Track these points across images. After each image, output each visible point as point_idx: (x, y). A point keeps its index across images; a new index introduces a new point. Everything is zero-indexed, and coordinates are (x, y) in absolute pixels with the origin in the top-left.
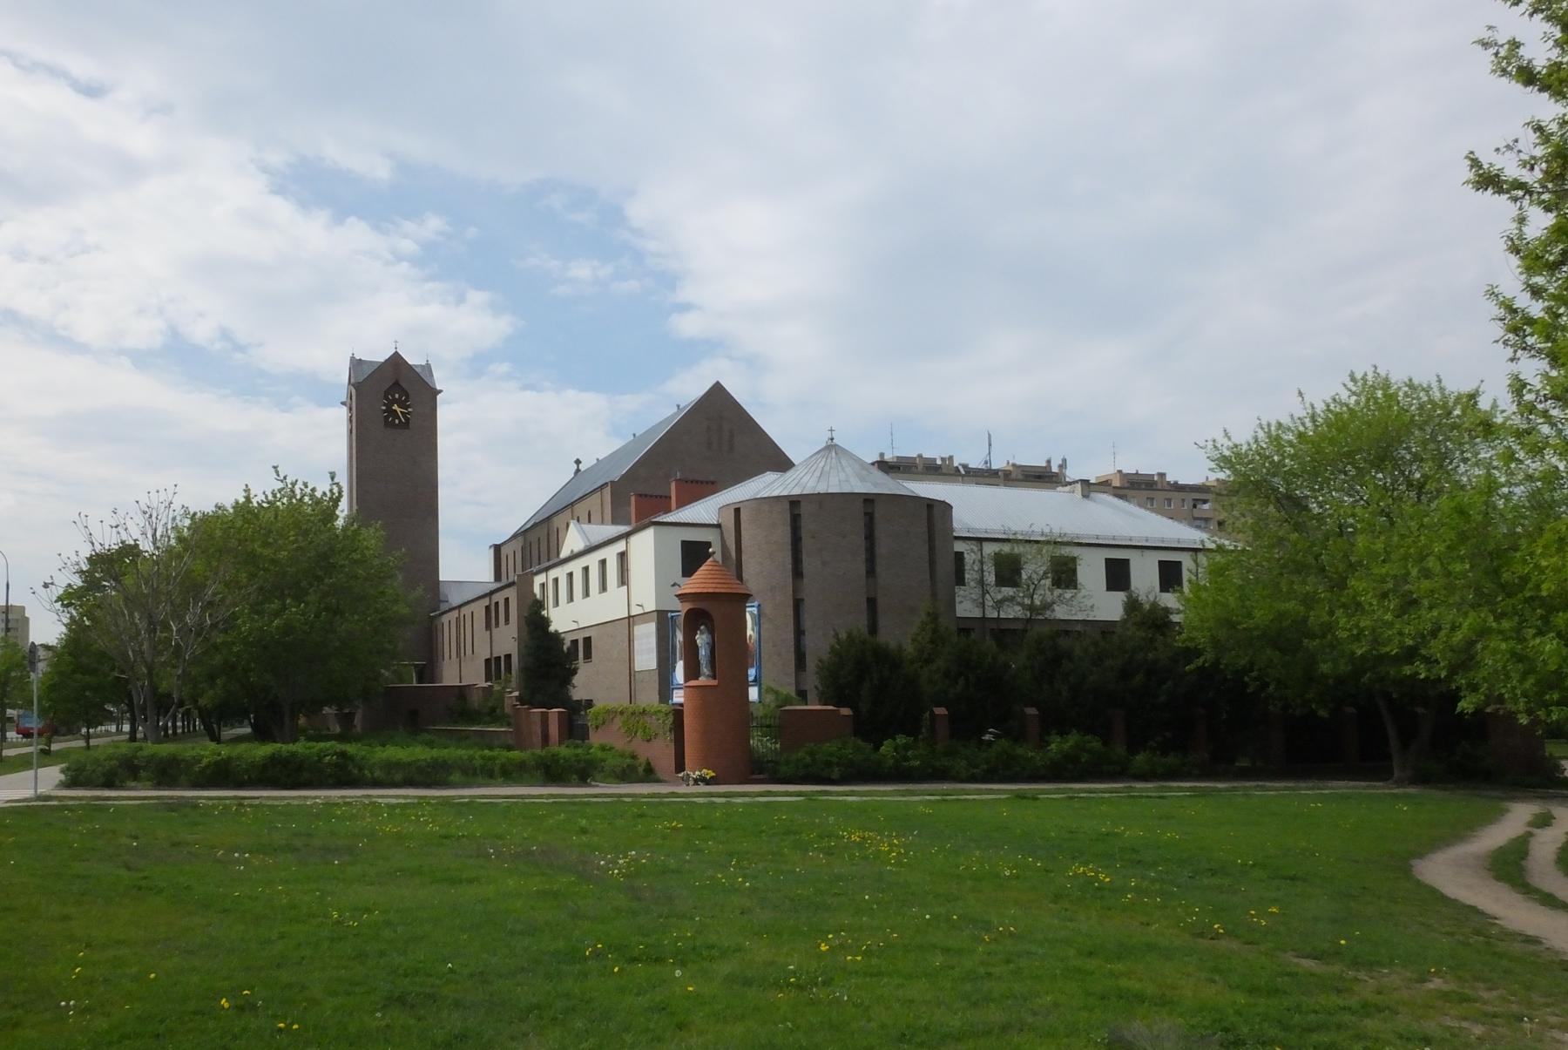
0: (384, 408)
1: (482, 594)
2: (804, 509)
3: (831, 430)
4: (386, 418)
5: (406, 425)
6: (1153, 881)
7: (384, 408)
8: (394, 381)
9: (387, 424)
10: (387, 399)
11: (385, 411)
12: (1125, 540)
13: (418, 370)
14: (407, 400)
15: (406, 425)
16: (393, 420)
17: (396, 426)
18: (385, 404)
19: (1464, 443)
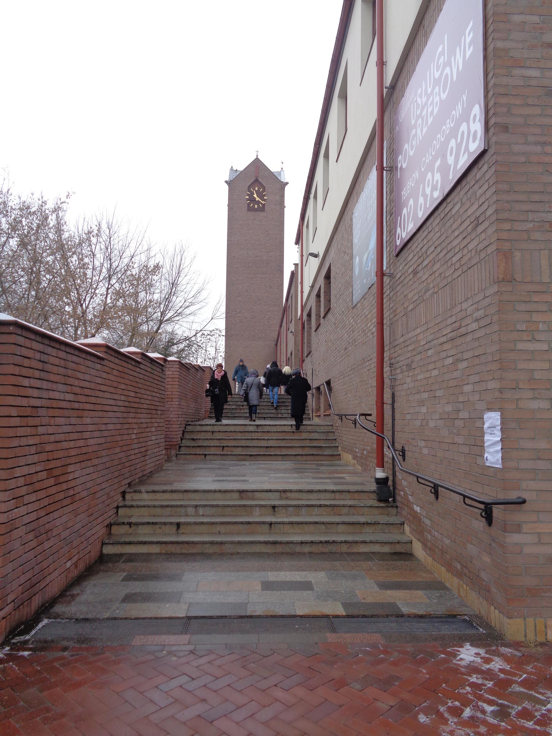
0: (247, 197)
1: (426, 17)
2: (483, 447)
3: (257, 151)
4: (249, 204)
5: (262, 209)
6: (440, 230)
7: (247, 197)
8: (254, 179)
9: (250, 209)
10: (249, 190)
11: (248, 200)
12: (391, 192)
13: (276, 174)
14: (264, 191)
15: (262, 209)
16: (254, 206)
17: (256, 210)
18: (248, 195)
19: (68, 270)
